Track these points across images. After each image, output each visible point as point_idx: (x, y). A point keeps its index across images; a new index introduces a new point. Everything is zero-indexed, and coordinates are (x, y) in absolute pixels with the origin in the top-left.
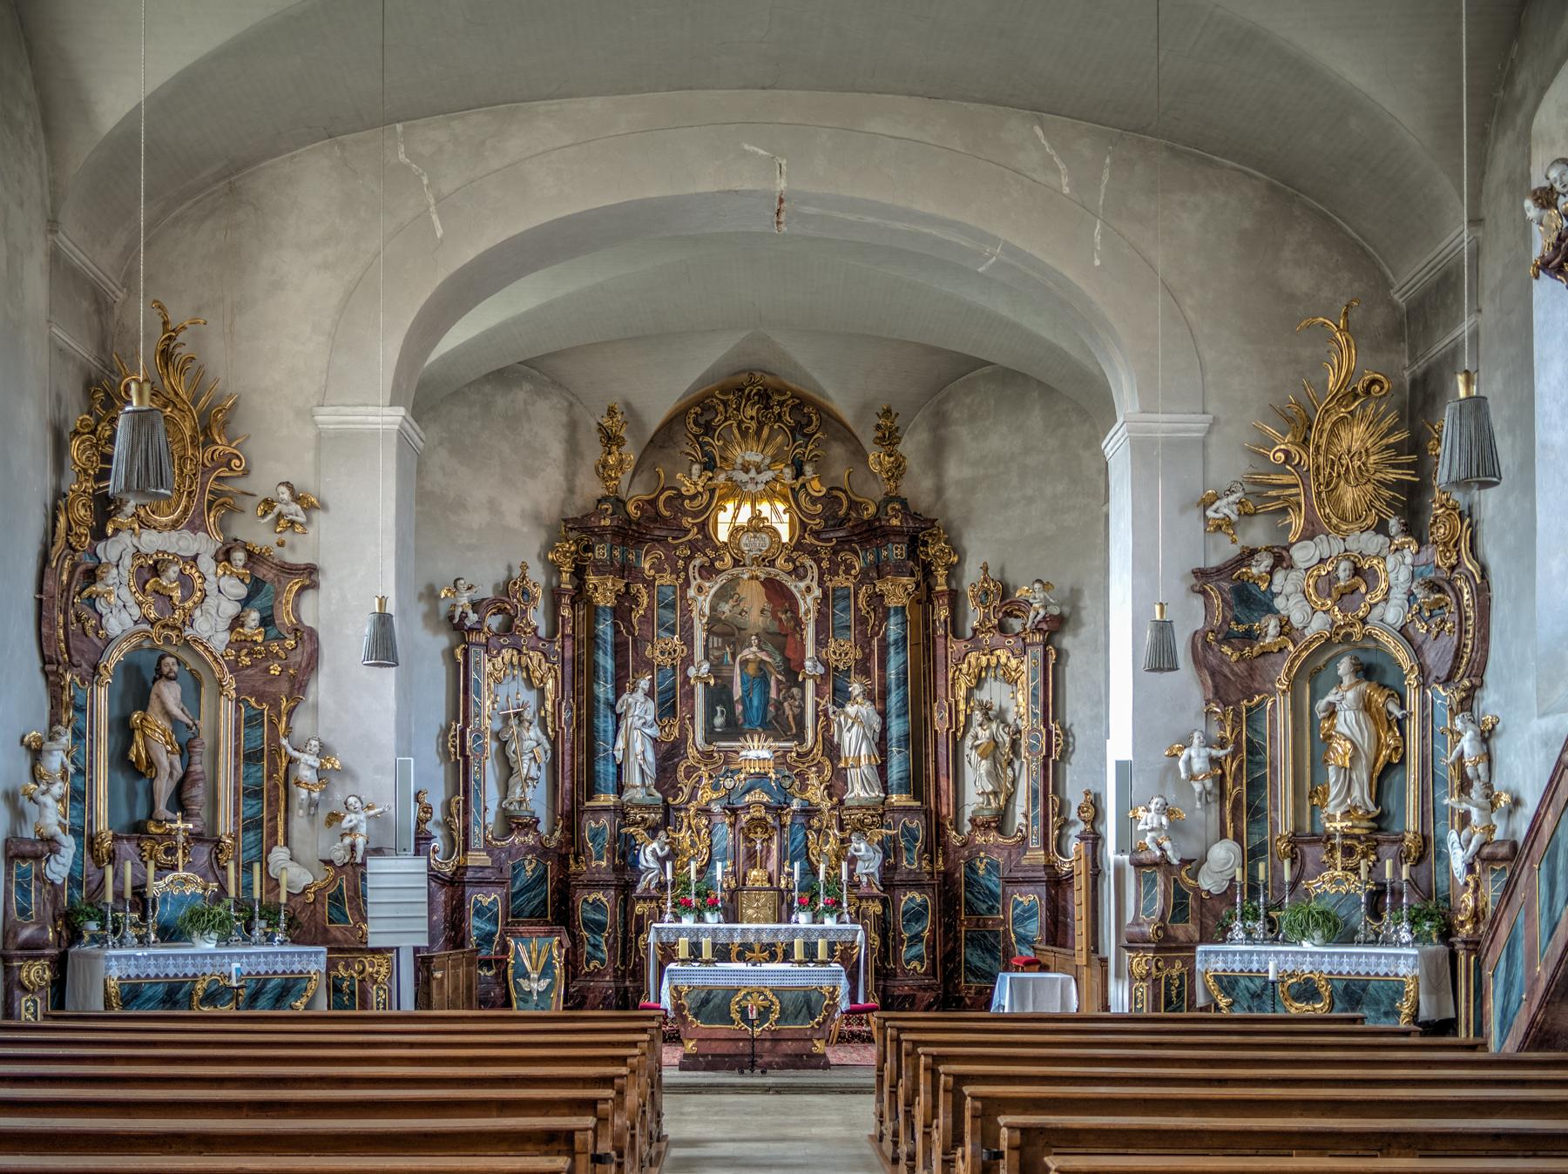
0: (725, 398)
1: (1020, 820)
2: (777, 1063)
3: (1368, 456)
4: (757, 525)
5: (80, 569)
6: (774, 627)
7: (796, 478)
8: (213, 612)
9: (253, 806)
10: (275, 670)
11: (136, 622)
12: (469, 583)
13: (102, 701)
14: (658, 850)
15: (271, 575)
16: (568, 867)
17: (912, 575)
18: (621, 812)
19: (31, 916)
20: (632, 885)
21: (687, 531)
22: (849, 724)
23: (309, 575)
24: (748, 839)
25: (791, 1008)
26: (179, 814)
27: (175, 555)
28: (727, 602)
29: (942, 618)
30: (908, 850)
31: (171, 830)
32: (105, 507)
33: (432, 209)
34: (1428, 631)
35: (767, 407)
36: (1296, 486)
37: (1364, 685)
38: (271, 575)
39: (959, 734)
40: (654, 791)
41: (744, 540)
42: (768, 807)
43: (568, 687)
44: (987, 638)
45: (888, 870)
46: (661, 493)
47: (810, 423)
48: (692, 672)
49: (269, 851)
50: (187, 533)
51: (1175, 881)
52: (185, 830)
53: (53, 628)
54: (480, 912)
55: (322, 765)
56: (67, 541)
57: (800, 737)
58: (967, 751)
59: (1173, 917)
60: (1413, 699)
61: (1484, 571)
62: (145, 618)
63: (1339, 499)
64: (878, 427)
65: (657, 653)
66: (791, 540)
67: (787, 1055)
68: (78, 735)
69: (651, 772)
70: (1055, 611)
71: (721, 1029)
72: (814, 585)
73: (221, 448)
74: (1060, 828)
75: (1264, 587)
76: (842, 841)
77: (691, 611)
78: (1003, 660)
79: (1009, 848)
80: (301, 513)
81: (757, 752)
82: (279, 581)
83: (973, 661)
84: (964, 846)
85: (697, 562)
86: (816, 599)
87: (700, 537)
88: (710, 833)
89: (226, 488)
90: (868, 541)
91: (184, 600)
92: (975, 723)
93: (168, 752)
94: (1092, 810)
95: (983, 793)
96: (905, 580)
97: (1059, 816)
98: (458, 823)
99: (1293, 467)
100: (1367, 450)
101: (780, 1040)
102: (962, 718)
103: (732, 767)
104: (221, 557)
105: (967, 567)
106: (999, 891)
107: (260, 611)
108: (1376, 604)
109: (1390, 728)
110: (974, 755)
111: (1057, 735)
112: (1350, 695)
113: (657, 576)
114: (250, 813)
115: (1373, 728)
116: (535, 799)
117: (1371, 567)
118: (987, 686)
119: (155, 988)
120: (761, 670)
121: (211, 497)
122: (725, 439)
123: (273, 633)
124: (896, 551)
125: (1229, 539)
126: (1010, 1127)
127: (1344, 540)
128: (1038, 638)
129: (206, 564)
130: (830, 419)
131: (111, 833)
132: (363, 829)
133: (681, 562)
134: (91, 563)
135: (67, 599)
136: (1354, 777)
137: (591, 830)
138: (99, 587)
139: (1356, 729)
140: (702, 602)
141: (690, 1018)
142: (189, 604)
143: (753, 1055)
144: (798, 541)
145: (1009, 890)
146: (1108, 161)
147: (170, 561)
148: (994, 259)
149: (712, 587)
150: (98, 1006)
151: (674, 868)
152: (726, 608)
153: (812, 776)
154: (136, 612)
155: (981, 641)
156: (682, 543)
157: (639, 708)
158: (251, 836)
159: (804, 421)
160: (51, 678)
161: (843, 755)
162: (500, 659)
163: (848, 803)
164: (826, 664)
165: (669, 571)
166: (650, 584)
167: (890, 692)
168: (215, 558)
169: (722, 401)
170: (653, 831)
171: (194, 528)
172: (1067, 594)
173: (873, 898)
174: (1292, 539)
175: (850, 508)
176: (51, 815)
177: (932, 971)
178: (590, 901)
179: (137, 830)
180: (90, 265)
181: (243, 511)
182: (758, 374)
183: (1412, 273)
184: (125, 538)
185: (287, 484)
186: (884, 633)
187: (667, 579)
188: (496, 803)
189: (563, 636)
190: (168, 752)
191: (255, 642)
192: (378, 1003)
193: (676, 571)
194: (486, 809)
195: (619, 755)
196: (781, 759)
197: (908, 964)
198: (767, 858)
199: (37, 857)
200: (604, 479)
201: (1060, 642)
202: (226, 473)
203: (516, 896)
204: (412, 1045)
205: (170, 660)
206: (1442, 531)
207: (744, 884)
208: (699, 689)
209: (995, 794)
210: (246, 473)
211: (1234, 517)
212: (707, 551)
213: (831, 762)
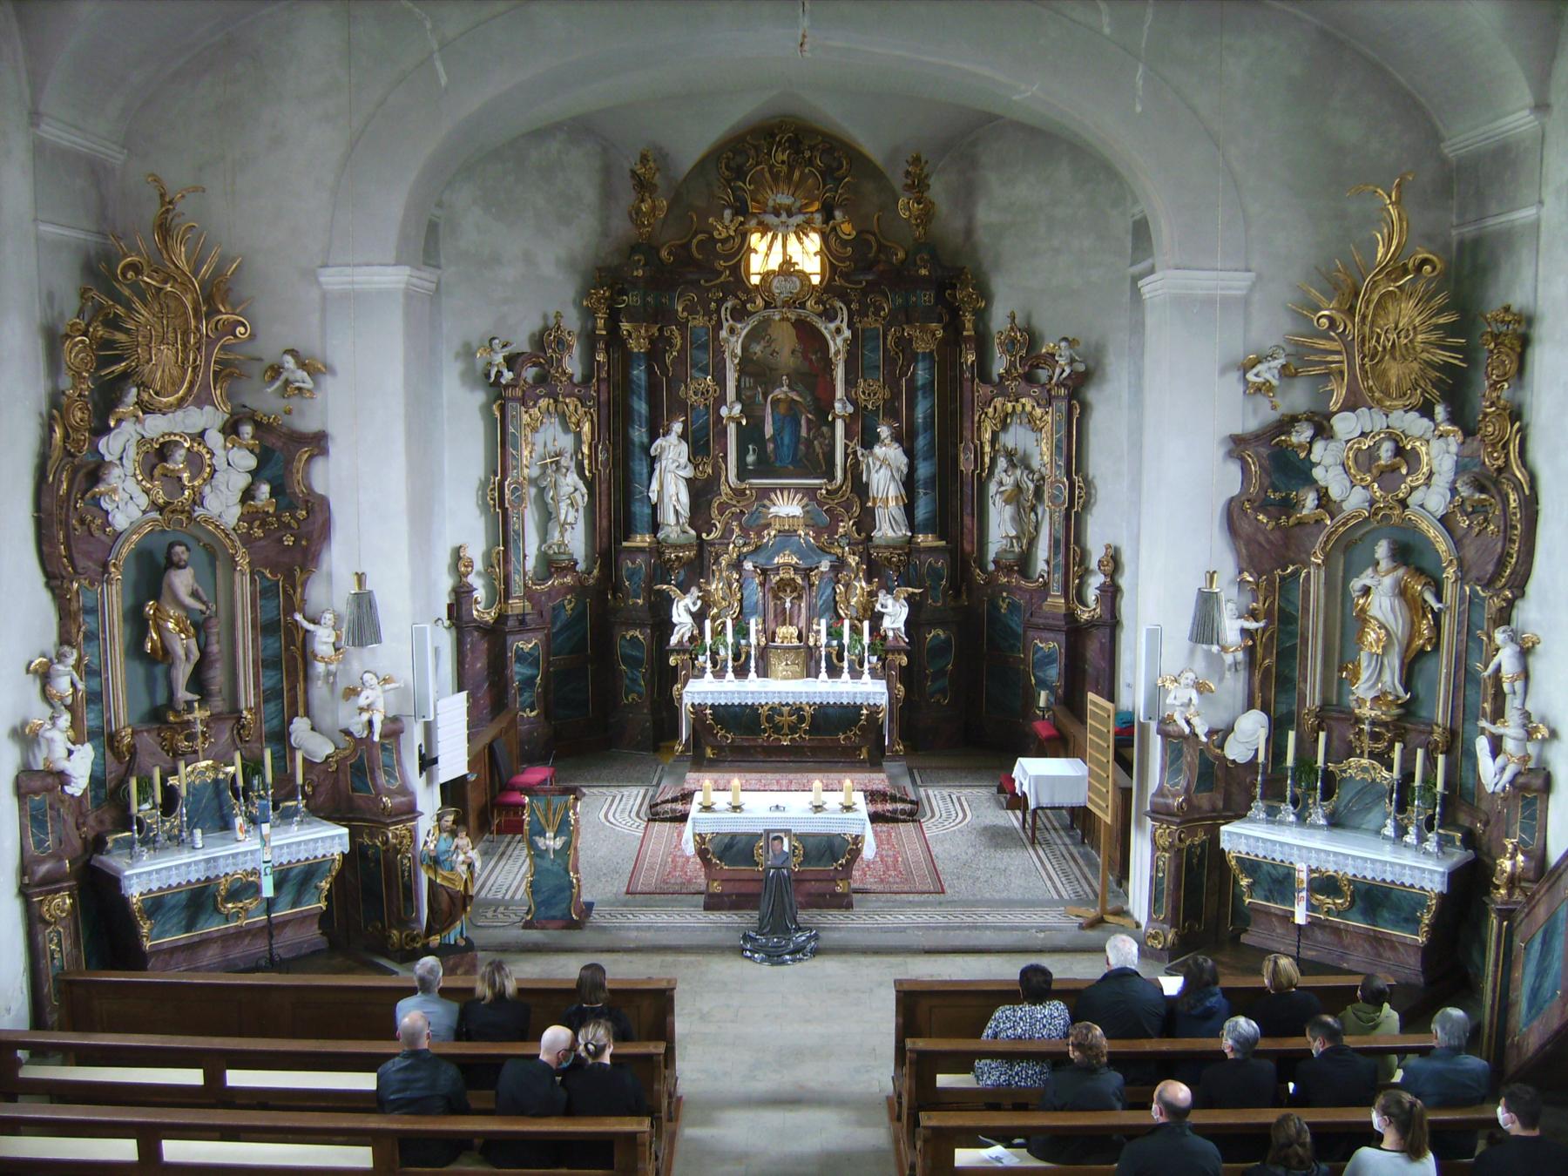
0: (756, 143)
1: (1041, 566)
3: (1415, 334)
9: (272, 677)
10: (289, 541)
11: (144, 512)
12: (504, 340)
13: (115, 598)
21: (720, 274)
24: (776, 597)
28: (759, 343)
29: (969, 362)
31: (189, 721)
35: (798, 152)
36: (1339, 353)
37: (1401, 572)
38: (280, 444)
40: (689, 529)
41: (775, 283)
42: (796, 569)
44: (1012, 385)
46: (693, 238)
48: (724, 411)
49: (290, 722)
53: (54, 546)
54: (521, 657)
56: (65, 448)
57: (832, 478)
59: (1197, 788)
61: (1533, 480)
63: (1384, 373)
64: (908, 173)
67: (810, 895)
69: (685, 511)
70: (1081, 368)
72: (844, 326)
73: (225, 317)
74: (1081, 577)
75: (1302, 455)
77: (724, 352)
78: (1028, 408)
79: (1032, 592)
83: (999, 406)
85: (729, 304)
86: (845, 340)
87: (731, 279)
94: (1111, 564)
95: (1007, 536)
99: (1337, 334)
100: (1415, 328)
102: (987, 460)
104: (229, 431)
106: (1020, 631)
108: (1417, 488)
109: (1424, 616)
111: (1079, 487)
112: (1388, 581)
113: (690, 317)
115: (1407, 615)
116: (575, 541)
117: (1413, 448)
118: (1012, 430)
119: (177, 897)
124: (926, 298)
125: (1269, 406)
127: (1387, 416)
128: (1063, 391)
129: (215, 439)
132: (380, 705)
136: (1386, 662)
137: (628, 569)
138: (102, 488)
139: (1391, 617)
140: (735, 345)
145: (1030, 633)
149: (744, 329)
152: (757, 349)
156: (714, 286)
157: (673, 451)
158: (272, 707)
159: (835, 165)
160: (57, 591)
161: (871, 495)
164: (854, 403)
165: (702, 313)
166: (682, 326)
168: (223, 430)
171: (199, 404)
173: (898, 651)
181: (249, 377)
184: (128, 427)
185: (292, 352)
193: (708, 313)
194: (525, 556)
195: (654, 497)
208: (732, 429)
209: (1018, 538)
211: (1275, 382)
212: (739, 293)
213: (860, 498)
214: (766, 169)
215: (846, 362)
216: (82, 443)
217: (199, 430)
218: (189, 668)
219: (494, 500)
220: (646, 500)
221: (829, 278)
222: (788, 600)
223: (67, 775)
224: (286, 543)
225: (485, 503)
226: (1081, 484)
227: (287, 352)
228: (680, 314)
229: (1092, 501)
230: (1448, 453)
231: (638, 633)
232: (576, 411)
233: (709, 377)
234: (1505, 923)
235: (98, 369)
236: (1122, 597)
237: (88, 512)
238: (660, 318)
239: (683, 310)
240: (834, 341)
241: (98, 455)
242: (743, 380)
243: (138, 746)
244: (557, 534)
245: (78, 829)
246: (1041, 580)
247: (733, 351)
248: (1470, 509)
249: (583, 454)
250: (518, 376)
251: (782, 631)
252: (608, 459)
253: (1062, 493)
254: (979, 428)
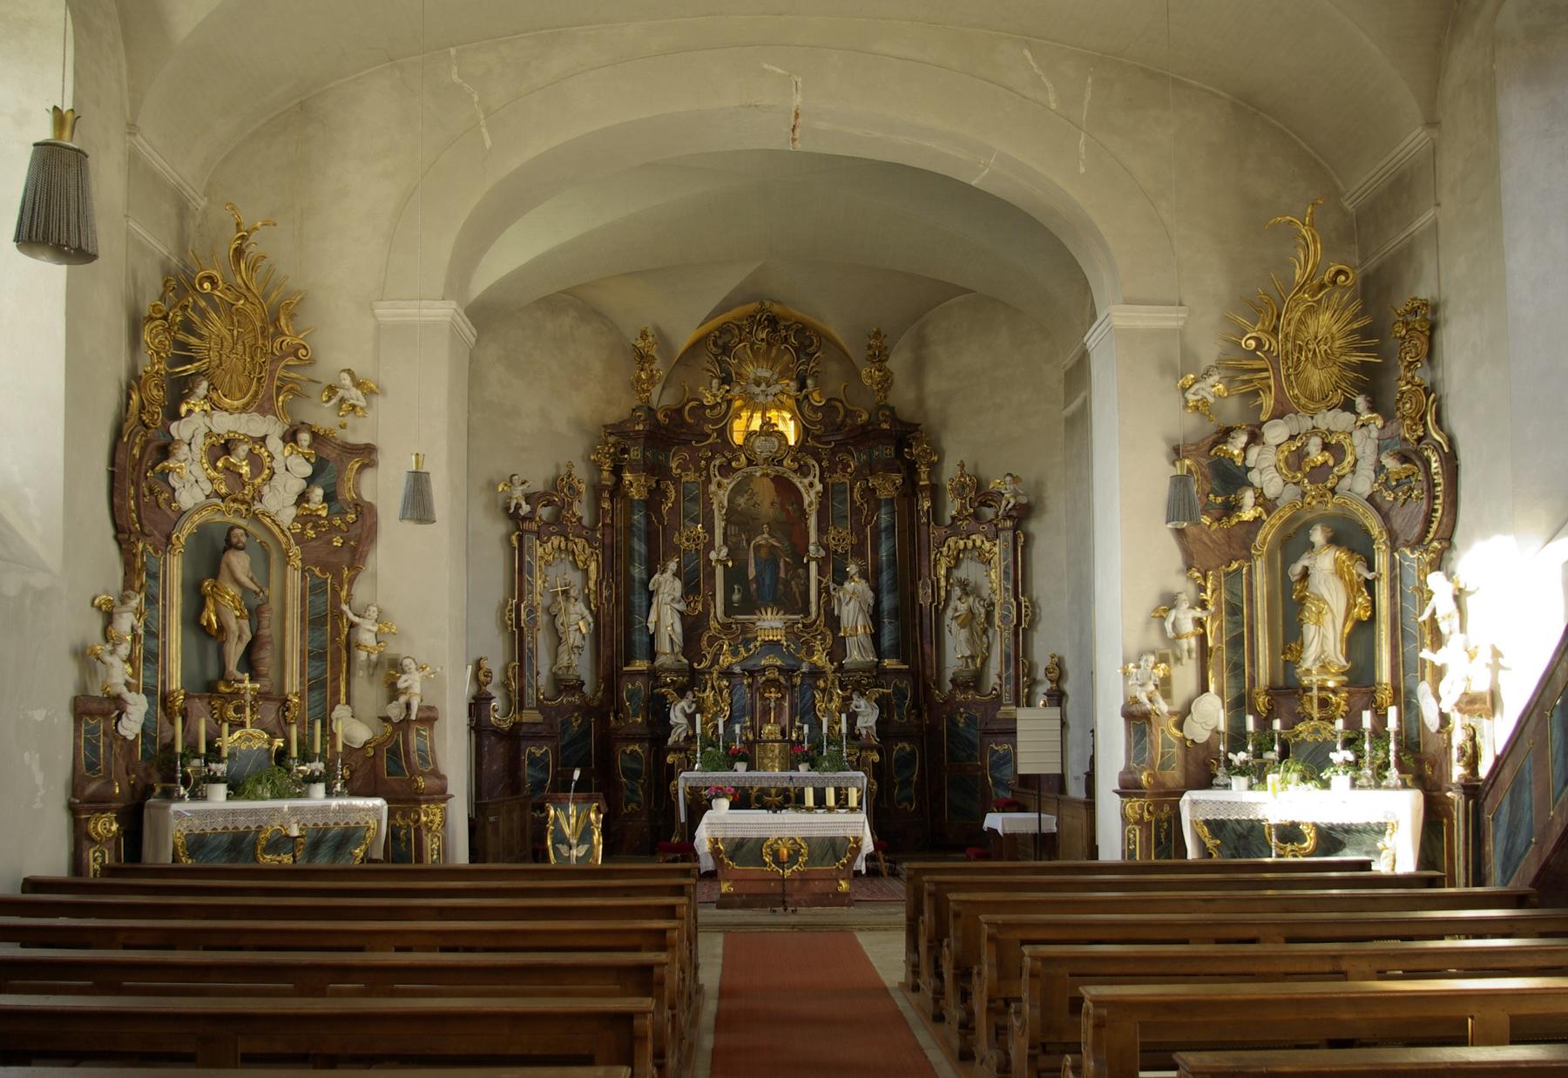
3: (1333, 342)
4: (769, 430)
5: (152, 446)
7: (800, 390)
8: (281, 489)
9: (317, 667)
10: (337, 542)
11: (207, 497)
13: (175, 569)
14: (686, 708)
15: (334, 455)
16: (609, 722)
18: (653, 675)
19: (99, 771)
21: (709, 436)
22: (848, 599)
23: (367, 454)
26: (247, 675)
27: (245, 435)
28: (742, 496)
29: (926, 508)
32: (179, 390)
33: (482, 122)
34: (1395, 499)
35: (775, 330)
36: (1266, 370)
40: (682, 658)
41: (757, 443)
42: (780, 669)
47: (811, 344)
48: (713, 555)
49: (332, 709)
50: (256, 416)
51: (1163, 731)
52: (253, 689)
53: (124, 498)
54: (534, 761)
55: (379, 629)
56: (140, 418)
57: (807, 613)
58: (947, 621)
60: (1382, 561)
61: (1451, 441)
62: (217, 494)
66: (796, 443)
68: (151, 600)
69: (678, 639)
70: (1024, 500)
72: (816, 481)
74: (1029, 687)
78: (978, 543)
80: (362, 398)
81: (770, 624)
82: (342, 460)
83: (952, 544)
85: (717, 462)
86: (818, 493)
89: (294, 375)
91: (254, 475)
93: (237, 617)
94: (1057, 671)
96: (894, 476)
99: (1264, 353)
101: (808, 880)
102: (943, 593)
103: (749, 636)
104: (288, 439)
106: (977, 741)
107: (324, 488)
108: (1343, 476)
110: (954, 626)
114: (315, 673)
116: (582, 666)
118: (964, 566)
121: (279, 383)
122: (739, 359)
123: (336, 508)
124: (889, 451)
127: (1312, 418)
128: (1009, 523)
129: (275, 444)
130: (825, 339)
131: (183, 691)
134: (163, 441)
135: (139, 472)
137: (628, 691)
138: (171, 464)
140: (720, 495)
142: (258, 481)
143: (784, 894)
144: (802, 444)
146: (1089, 81)
147: (240, 440)
148: (987, 171)
149: (729, 483)
150: (166, 859)
152: (741, 501)
153: (818, 645)
154: (208, 488)
157: (668, 586)
158: (316, 695)
159: (807, 342)
160: (124, 546)
161: (842, 625)
162: (550, 544)
164: (826, 548)
167: (881, 572)
169: (737, 326)
170: (682, 694)
171: (263, 411)
173: (872, 748)
174: (1263, 418)
175: (846, 416)
176: (118, 673)
178: (628, 752)
179: (210, 689)
180: (170, 170)
182: (767, 304)
183: (1365, 179)
185: (349, 371)
187: (690, 477)
188: (548, 667)
190: (237, 617)
191: (319, 516)
192: (432, 850)
193: (698, 470)
194: (538, 673)
196: (789, 628)
199: (106, 715)
202: (292, 361)
203: (564, 747)
204: (442, 913)
205: (238, 532)
206: (1408, 406)
208: (719, 570)
209: (973, 657)
210: (312, 362)
213: (832, 631)
215: (819, 513)
216: (156, 417)
217: (262, 435)
218: (242, 648)
219: (511, 620)
220: (645, 630)
223: (123, 700)
224: (335, 544)
225: (503, 622)
227: (344, 371)
229: (1037, 618)
230: (1370, 438)
231: (637, 747)
233: (700, 525)
234: (1471, 802)
235: (172, 366)
237: (156, 483)
239: (676, 468)
240: (808, 493)
241: (168, 435)
243: (189, 710)
245: (128, 774)
248: (1394, 483)
249: (589, 590)
250: (533, 511)
252: (611, 595)
254: (935, 566)
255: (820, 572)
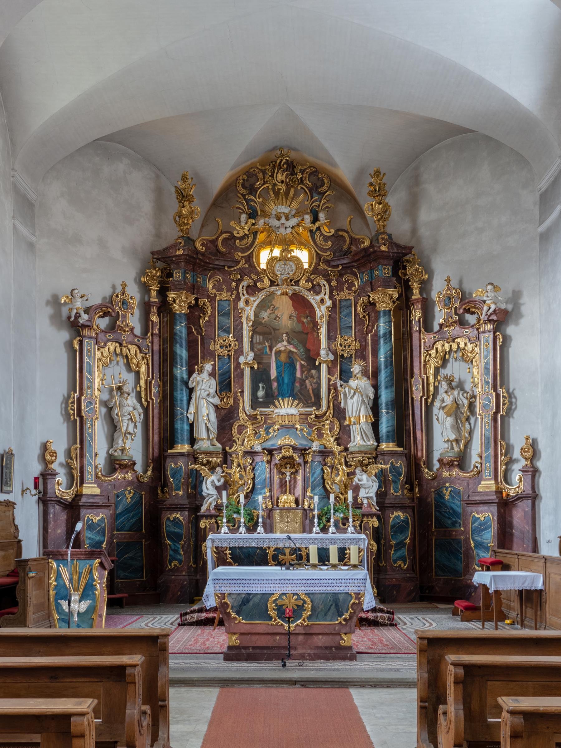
1: (474, 459)
2: (309, 655)
6: (299, 328)
12: (82, 293)
14: (216, 482)
17: (395, 288)
18: (194, 457)
20: (198, 508)
21: (239, 262)
25: (321, 607)
28: (266, 311)
30: (395, 482)
35: (293, 174)
39: (429, 400)
42: (295, 449)
43: (156, 371)
45: (381, 495)
47: (323, 185)
48: (242, 360)
57: (319, 406)
65: (218, 347)
66: (310, 266)
67: (318, 648)
69: (214, 428)
70: (503, 306)
71: (260, 625)
72: (327, 297)
74: (506, 464)
76: (349, 474)
77: (241, 317)
78: (462, 345)
83: (440, 347)
84: (434, 479)
85: (245, 283)
86: (328, 307)
88: (253, 468)
90: (364, 265)
92: (441, 391)
94: (531, 451)
95: (448, 441)
96: (391, 291)
97: (505, 455)
98: (76, 464)
102: (432, 389)
105: (434, 282)
111: (504, 397)
118: (449, 365)
120: (290, 358)
124: (386, 271)
126: (455, 664)
128: (489, 327)
133: (234, 284)
137: (172, 469)
140: (249, 312)
141: (233, 615)
143: (289, 648)
145: (469, 509)
149: (256, 300)
151: (228, 496)
152: (265, 315)
155: (445, 333)
156: (234, 270)
159: (319, 184)
162: (106, 349)
163: (351, 450)
164: (335, 353)
165: (226, 290)
166: (212, 299)
167: (380, 371)
172: (510, 295)
173: (372, 515)
175: (351, 244)
177: (412, 568)
186: (376, 331)
187: (224, 295)
189: (152, 335)
193: (230, 290)
195: (191, 417)
197: (395, 563)
198: (295, 487)
200: (180, 225)
201: (505, 330)
207: (278, 506)
208: (247, 372)
209: (457, 441)
212: (252, 275)
214: (270, 187)
215: (329, 323)
219: (73, 410)
221: (316, 264)
222: (288, 474)
226: (505, 394)
228: (210, 291)
229: (513, 407)
231: (178, 515)
232: (136, 355)
233: (231, 335)
236: (539, 476)
238: (196, 290)
239: (213, 288)
240: (319, 308)
242: (255, 337)
244: (120, 441)
246: (475, 469)
247: (248, 316)
251: (284, 498)
252: (159, 392)
253: (490, 402)
255: (330, 372)
